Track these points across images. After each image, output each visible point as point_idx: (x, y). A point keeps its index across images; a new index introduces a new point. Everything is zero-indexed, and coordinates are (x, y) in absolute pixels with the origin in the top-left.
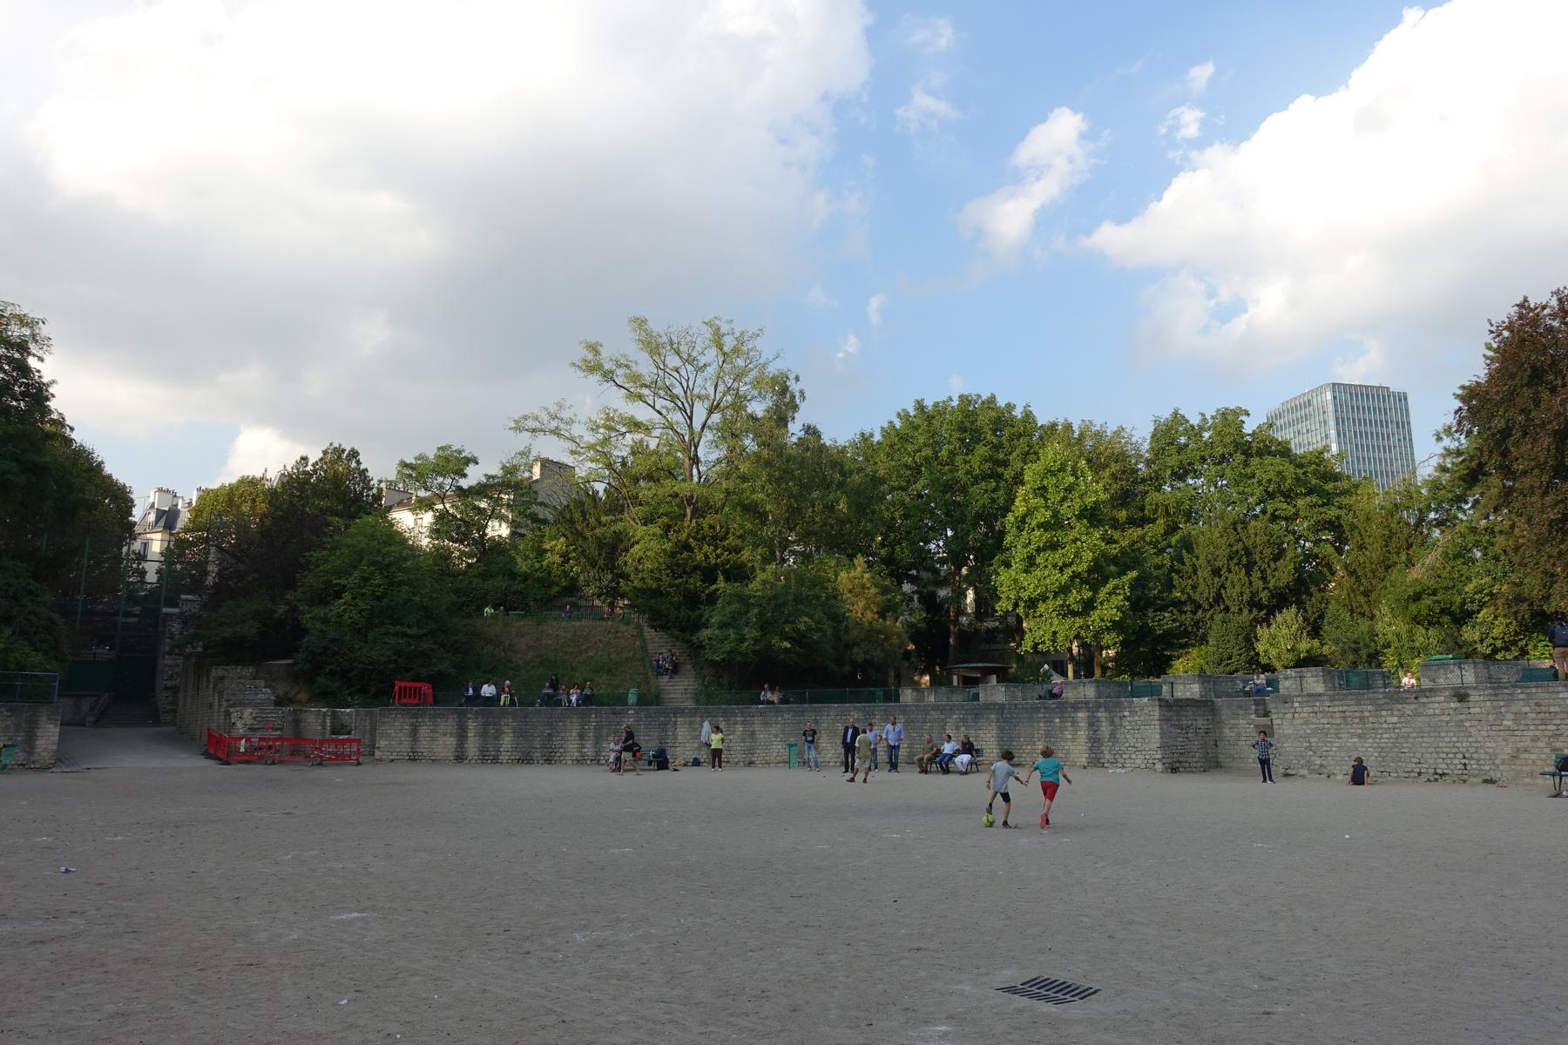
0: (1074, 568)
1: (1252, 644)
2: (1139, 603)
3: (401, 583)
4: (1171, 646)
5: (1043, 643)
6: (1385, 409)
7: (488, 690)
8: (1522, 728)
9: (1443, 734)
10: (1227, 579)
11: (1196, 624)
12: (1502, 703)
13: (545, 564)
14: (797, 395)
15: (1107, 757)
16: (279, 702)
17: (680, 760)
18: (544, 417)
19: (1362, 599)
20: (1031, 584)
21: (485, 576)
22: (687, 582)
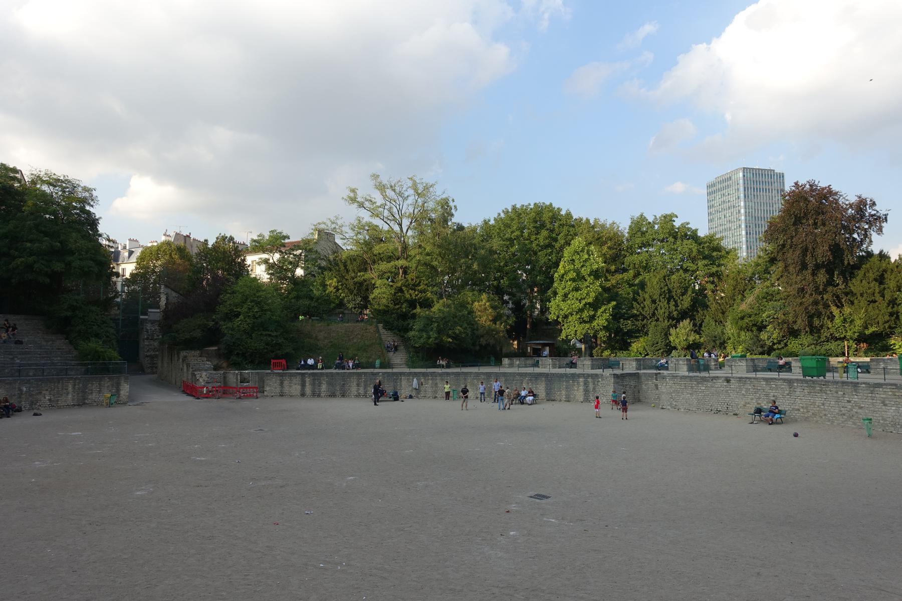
1: (668, 337)
2: (616, 316)
3: (266, 310)
4: (631, 337)
5: (570, 335)
6: (771, 183)
7: (311, 362)
8: (748, 394)
9: (721, 395)
10: (659, 305)
11: (643, 326)
12: (742, 384)
13: (327, 292)
14: (453, 208)
15: (592, 398)
16: (216, 368)
17: (403, 396)
18: (329, 223)
19: (720, 315)
21: (298, 298)
22: (401, 307)
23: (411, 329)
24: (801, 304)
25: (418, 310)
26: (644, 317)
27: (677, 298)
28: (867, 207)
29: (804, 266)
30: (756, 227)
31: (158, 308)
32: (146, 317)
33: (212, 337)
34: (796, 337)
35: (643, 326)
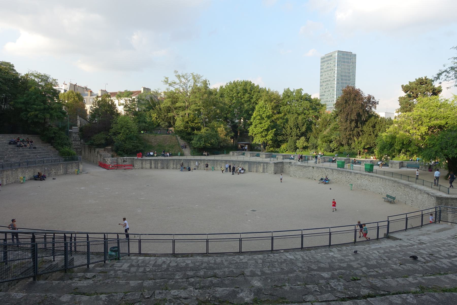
0: (264, 128)
2: (276, 134)
3: (131, 131)
6: (350, 59)
7: (152, 153)
11: (286, 138)
14: (208, 84)
16: (113, 156)
20: (256, 131)
23: (193, 140)
24: (345, 134)
25: (196, 132)
26: (287, 135)
27: (300, 127)
28: (371, 99)
29: (347, 120)
30: (341, 80)
31: (77, 126)
32: (72, 130)
33: (109, 142)
34: (343, 146)
35: (286, 138)
